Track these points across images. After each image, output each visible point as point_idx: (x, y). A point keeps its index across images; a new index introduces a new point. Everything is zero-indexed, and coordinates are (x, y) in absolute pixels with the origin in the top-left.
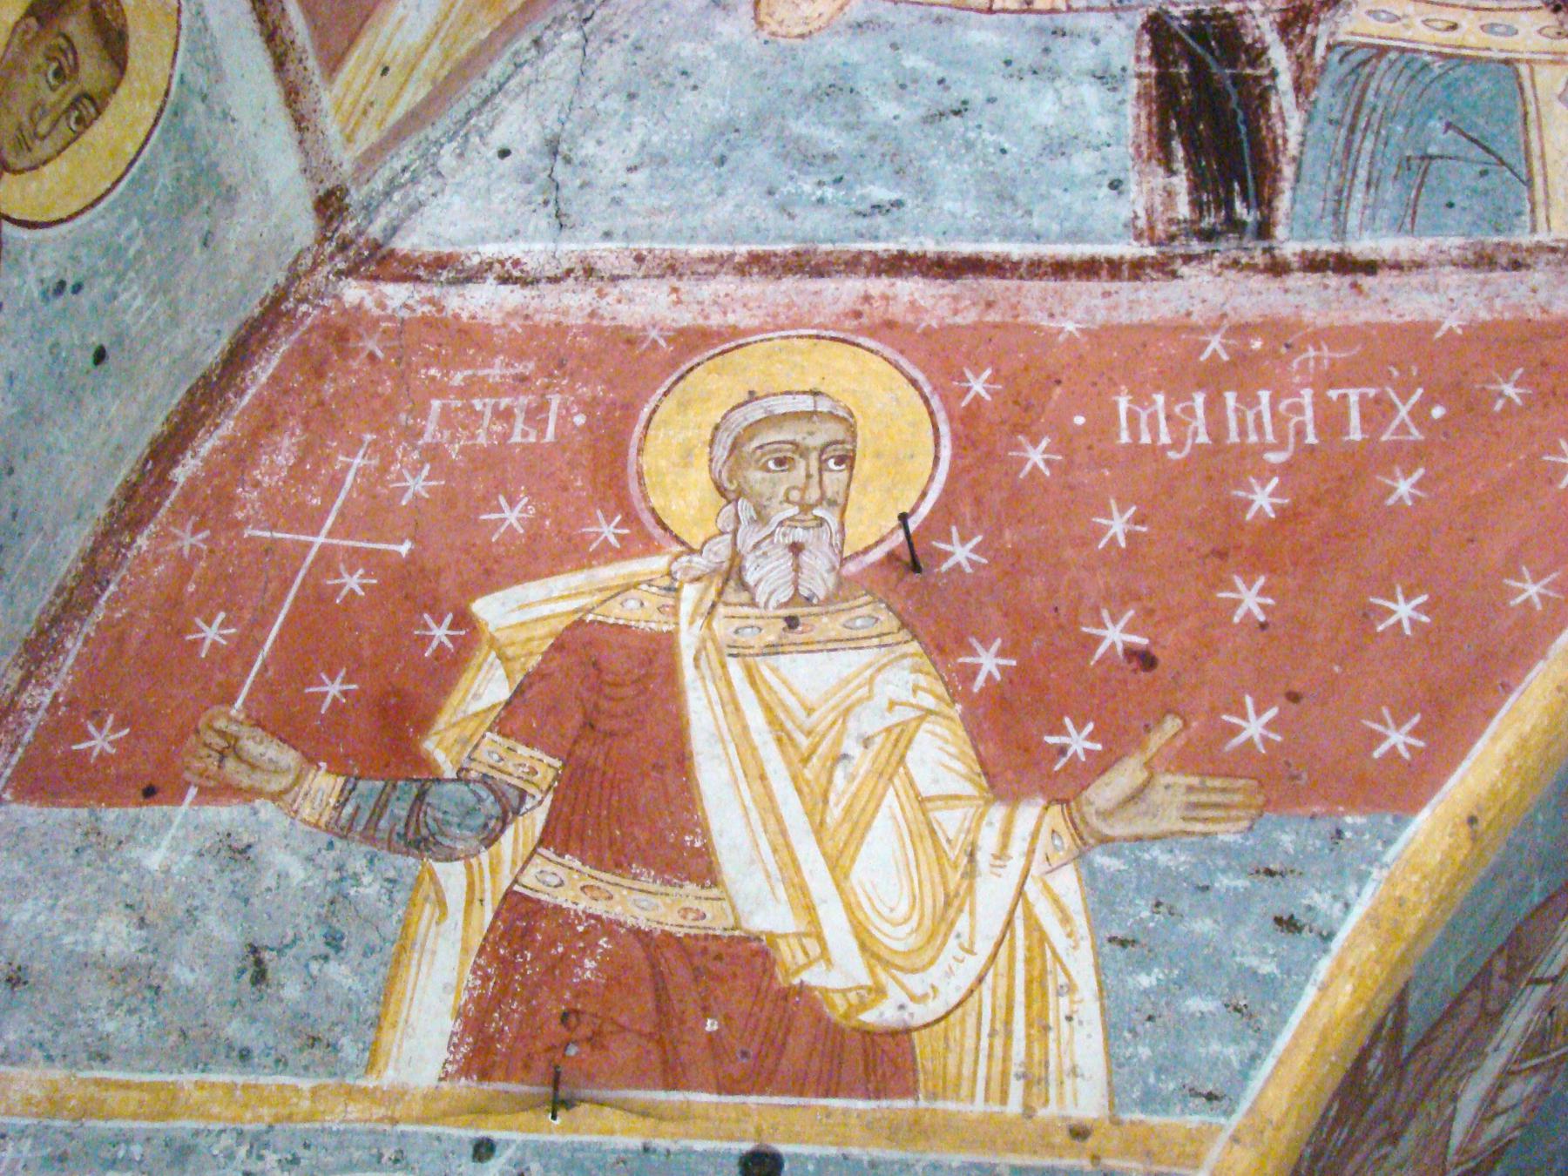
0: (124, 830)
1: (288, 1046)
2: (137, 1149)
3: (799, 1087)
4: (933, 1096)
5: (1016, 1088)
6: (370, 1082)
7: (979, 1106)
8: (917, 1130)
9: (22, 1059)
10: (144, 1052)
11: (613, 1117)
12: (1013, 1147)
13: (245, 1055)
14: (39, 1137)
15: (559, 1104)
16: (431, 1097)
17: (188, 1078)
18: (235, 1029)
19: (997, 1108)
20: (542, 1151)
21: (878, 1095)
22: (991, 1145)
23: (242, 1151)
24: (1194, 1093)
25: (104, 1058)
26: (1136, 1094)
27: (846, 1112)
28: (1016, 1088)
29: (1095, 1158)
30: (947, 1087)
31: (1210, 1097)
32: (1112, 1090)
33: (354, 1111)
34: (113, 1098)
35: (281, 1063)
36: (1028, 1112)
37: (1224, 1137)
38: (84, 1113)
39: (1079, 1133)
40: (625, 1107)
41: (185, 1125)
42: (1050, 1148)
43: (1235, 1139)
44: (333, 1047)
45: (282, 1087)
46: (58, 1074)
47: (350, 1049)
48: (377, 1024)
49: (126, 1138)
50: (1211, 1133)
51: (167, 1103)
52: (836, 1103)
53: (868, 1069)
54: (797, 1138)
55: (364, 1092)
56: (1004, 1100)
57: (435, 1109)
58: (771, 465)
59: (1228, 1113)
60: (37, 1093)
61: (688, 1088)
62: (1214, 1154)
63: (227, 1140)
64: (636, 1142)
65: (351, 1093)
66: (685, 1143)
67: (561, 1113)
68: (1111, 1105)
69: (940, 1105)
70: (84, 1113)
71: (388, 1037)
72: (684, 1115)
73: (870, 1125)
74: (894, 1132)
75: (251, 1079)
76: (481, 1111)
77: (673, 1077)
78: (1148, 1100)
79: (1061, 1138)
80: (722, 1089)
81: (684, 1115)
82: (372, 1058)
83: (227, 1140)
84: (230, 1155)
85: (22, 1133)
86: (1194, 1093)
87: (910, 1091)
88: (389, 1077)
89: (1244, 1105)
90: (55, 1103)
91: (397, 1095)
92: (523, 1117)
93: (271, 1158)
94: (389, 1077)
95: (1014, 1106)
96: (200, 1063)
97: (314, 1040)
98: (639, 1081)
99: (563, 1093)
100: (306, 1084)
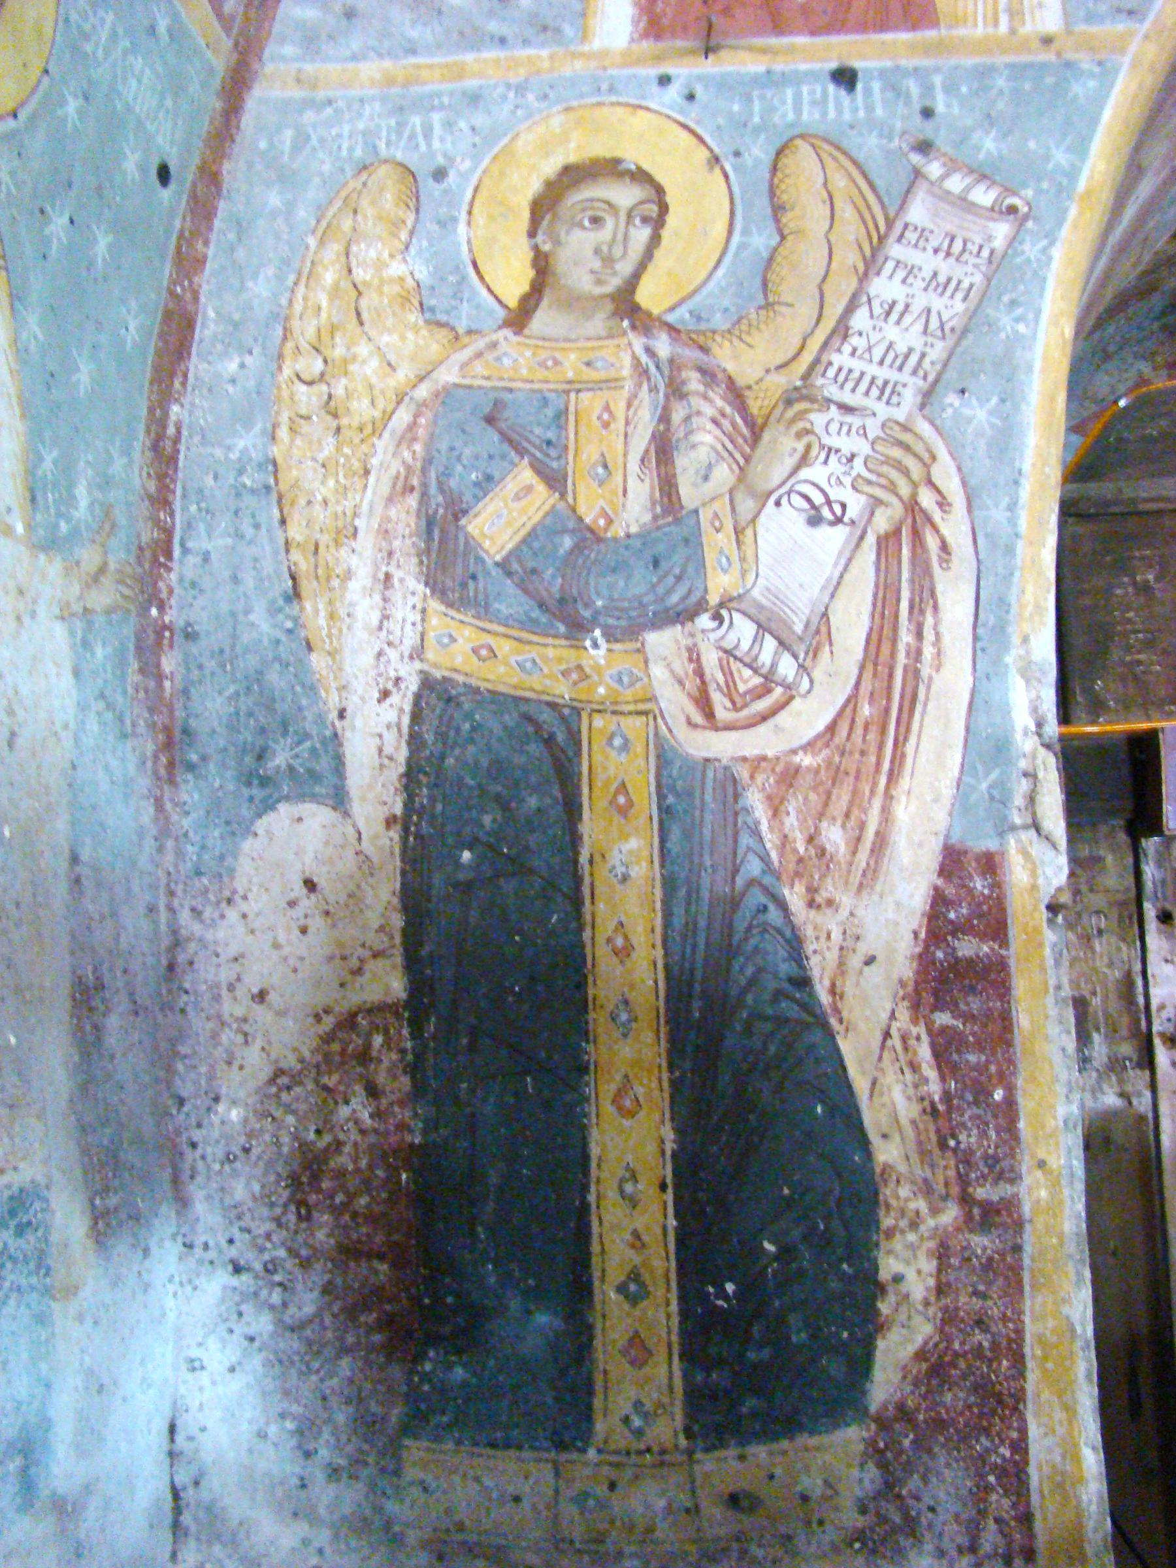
0: (375, 966)
1: (529, 32)
2: (446, 100)
3: (863, 27)
4: (950, 27)
5: (1004, 20)
6: (586, 48)
7: (980, 30)
8: (940, 48)
9: (365, 58)
10: (439, 47)
11: (743, 55)
12: (1004, 52)
13: (503, 41)
14: (384, 100)
15: (708, 51)
16: (626, 54)
17: (469, 57)
18: (493, 26)
19: (990, 30)
20: (700, 78)
21: (914, 28)
22: (990, 52)
23: (512, 94)
24: (1119, 10)
25: (413, 52)
26: (1082, 14)
27: (894, 42)
28: (1004, 20)
29: (1058, 54)
30: (958, 21)
31: (1130, 13)
32: (1066, 13)
33: (578, 65)
34: (425, 74)
35: (526, 42)
36: (1013, 31)
37: (1138, 38)
38: (407, 83)
39: (1047, 41)
40: (750, 49)
41: (472, 84)
42: (1029, 51)
43: (1146, 37)
44: (558, 31)
45: (529, 58)
46: (387, 64)
47: (569, 31)
48: (584, 15)
49: (439, 95)
50: (1132, 34)
51: (460, 72)
52: (888, 37)
53: (906, 13)
54: (864, 57)
55: (582, 55)
56: (996, 23)
57: (628, 59)
58: (586, 223)
59: (1142, 21)
60: (378, 76)
61: (791, 33)
62: (1133, 47)
63: (501, 90)
64: (761, 69)
65: (574, 55)
66: (792, 67)
67: (711, 57)
68: (1067, 23)
69: (955, 32)
70: (407, 83)
71: (591, 22)
72: (791, 50)
73: (912, 47)
74: (927, 50)
75: (508, 53)
76: (659, 58)
77: (778, 26)
78: (1090, 18)
79: (1036, 44)
80: (813, 33)
81: (791, 50)
82: (584, 35)
83: (501, 90)
84: (504, 98)
85: (373, 99)
86: (1119, 10)
87: (934, 24)
88: (596, 44)
89: (1151, 17)
90: (390, 81)
91: (604, 54)
92: (686, 60)
93: (531, 97)
94: (596, 44)
95: (1003, 27)
96: (475, 47)
97: (545, 29)
98: (759, 33)
99: (713, 43)
100: (544, 53)
